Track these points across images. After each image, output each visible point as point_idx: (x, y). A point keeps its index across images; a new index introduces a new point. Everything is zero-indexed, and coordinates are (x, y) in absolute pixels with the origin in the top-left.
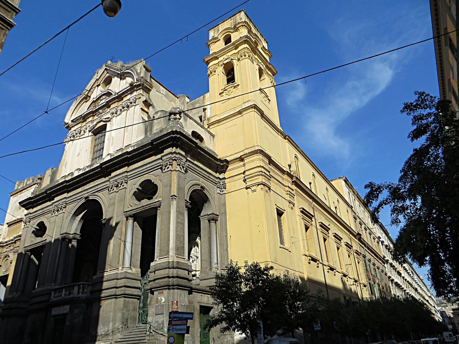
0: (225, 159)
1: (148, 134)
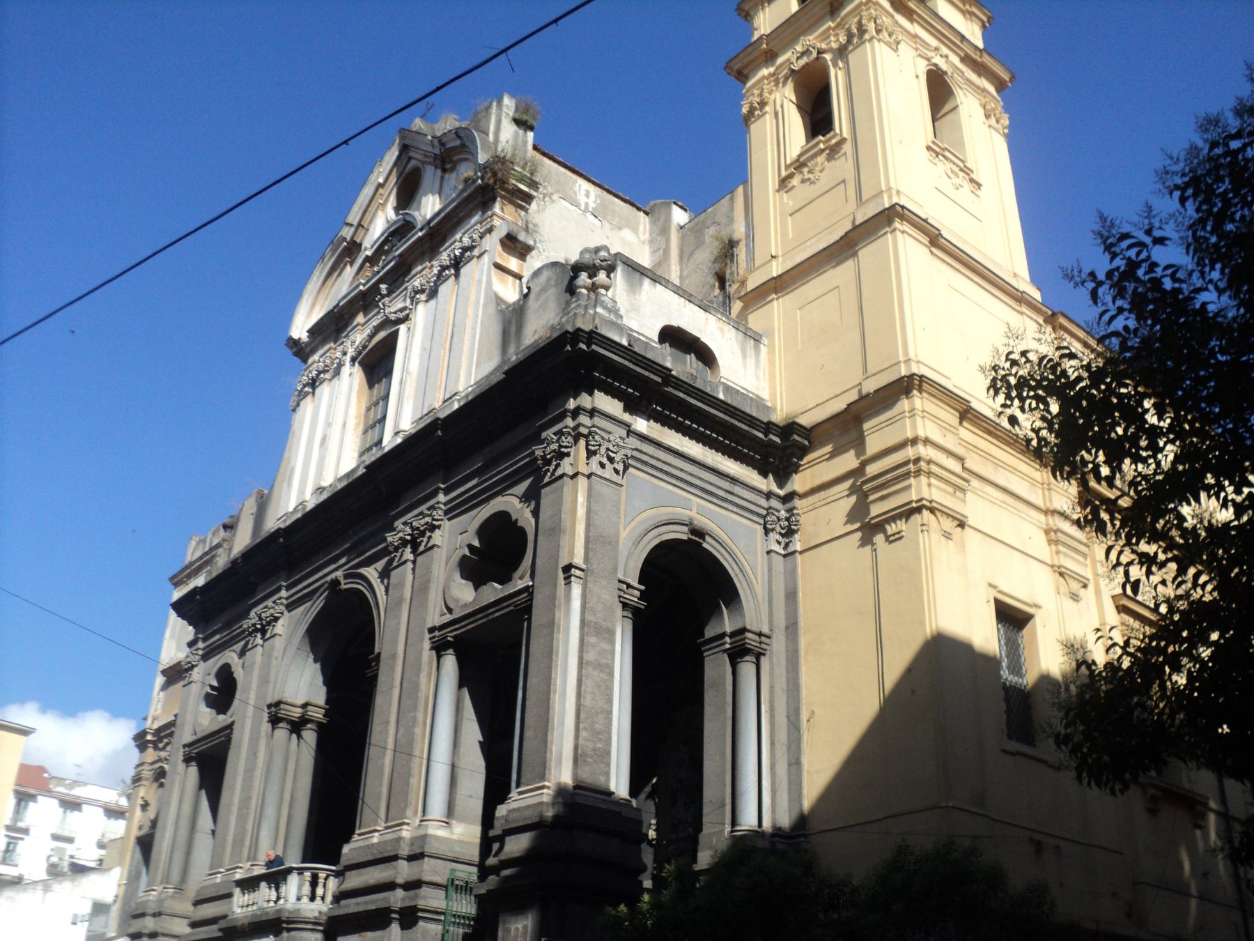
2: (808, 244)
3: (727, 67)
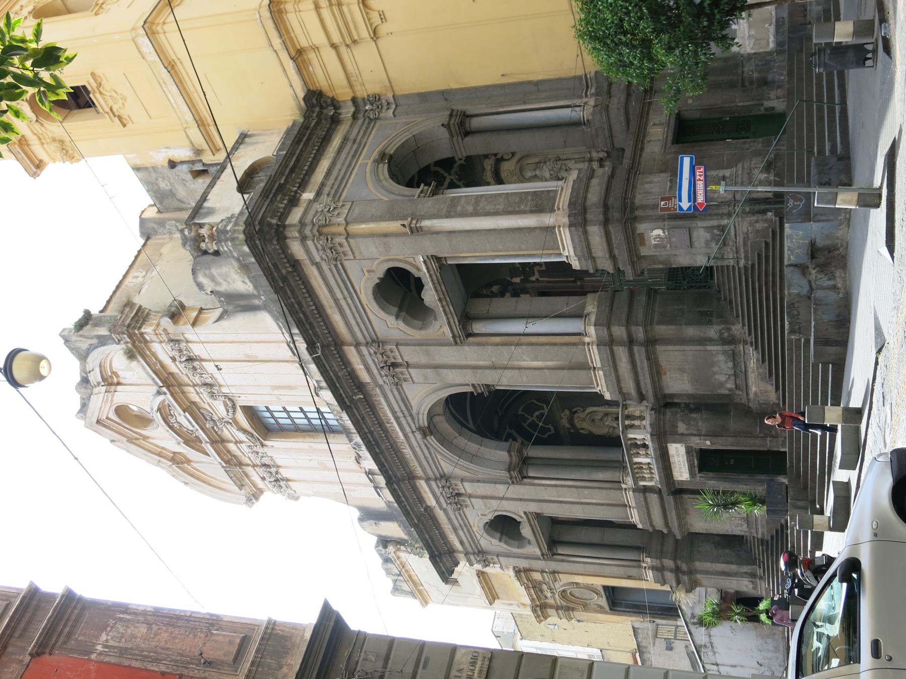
0: (302, 103)
1: (257, 302)
3: (34, 175)
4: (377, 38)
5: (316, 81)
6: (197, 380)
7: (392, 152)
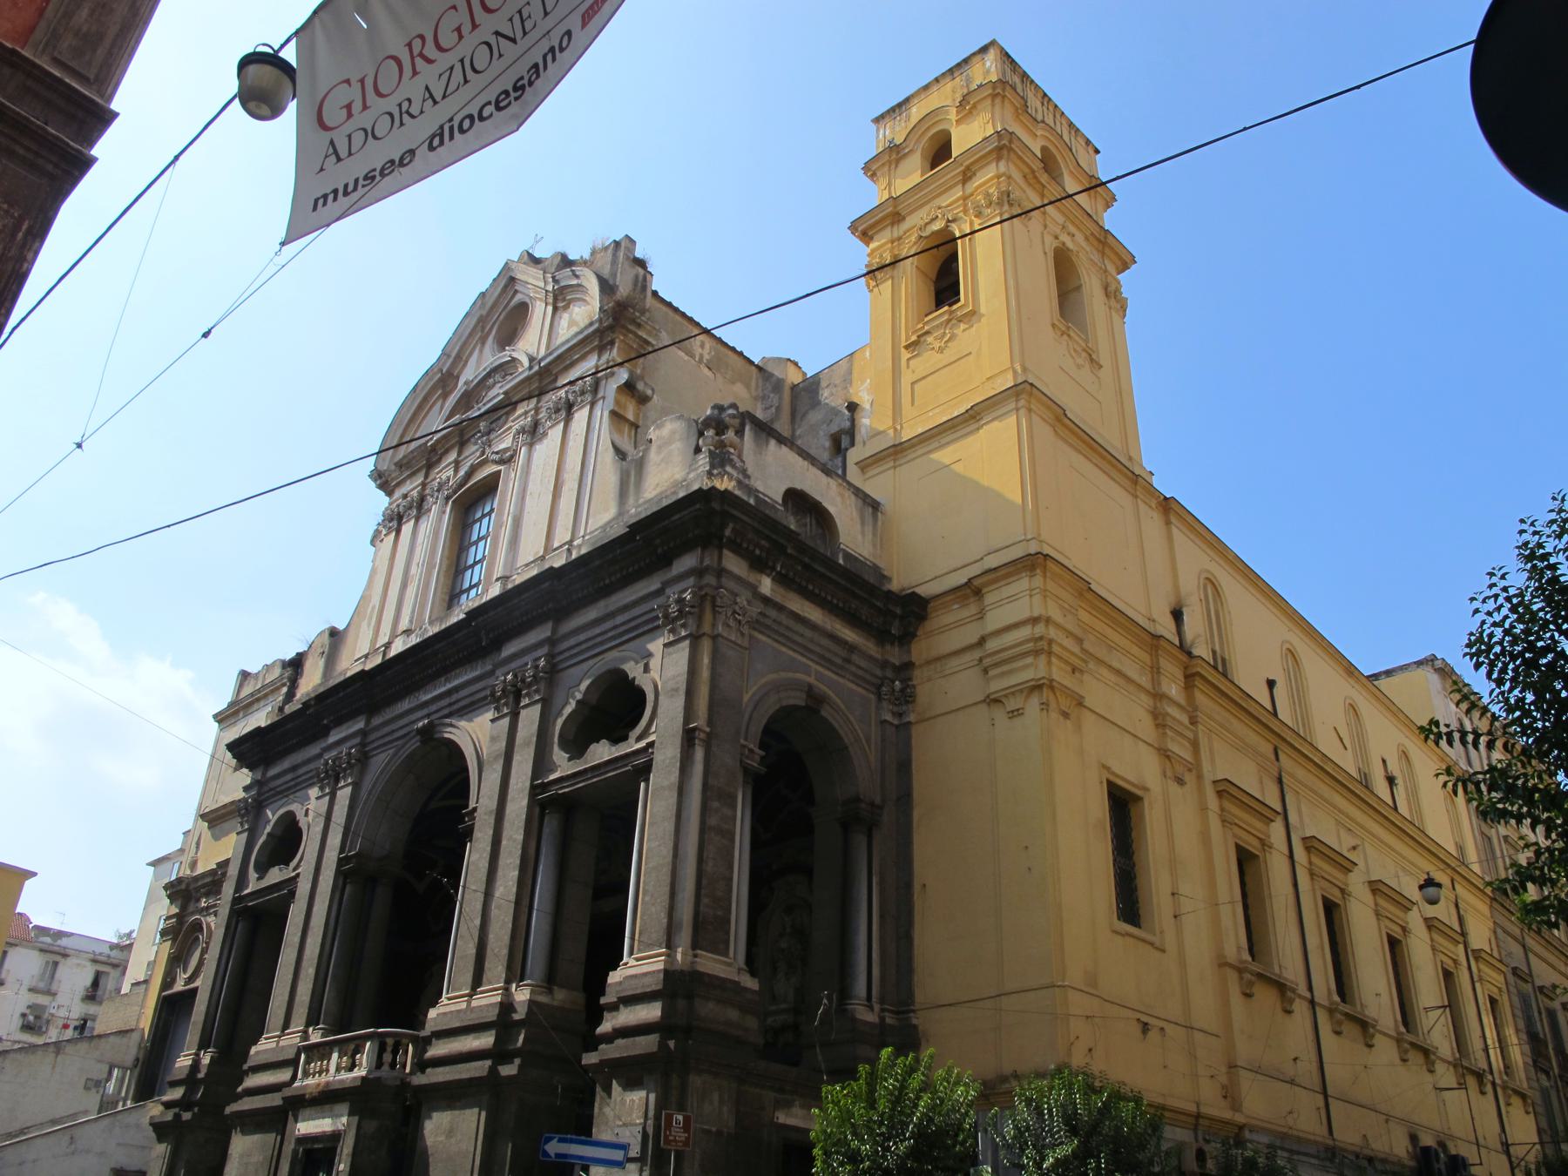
0: (910, 591)
1: (631, 501)
2: (931, 414)
3: (853, 227)
4: (989, 704)
5: (939, 613)
6: (543, 415)
7: (823, 713)
